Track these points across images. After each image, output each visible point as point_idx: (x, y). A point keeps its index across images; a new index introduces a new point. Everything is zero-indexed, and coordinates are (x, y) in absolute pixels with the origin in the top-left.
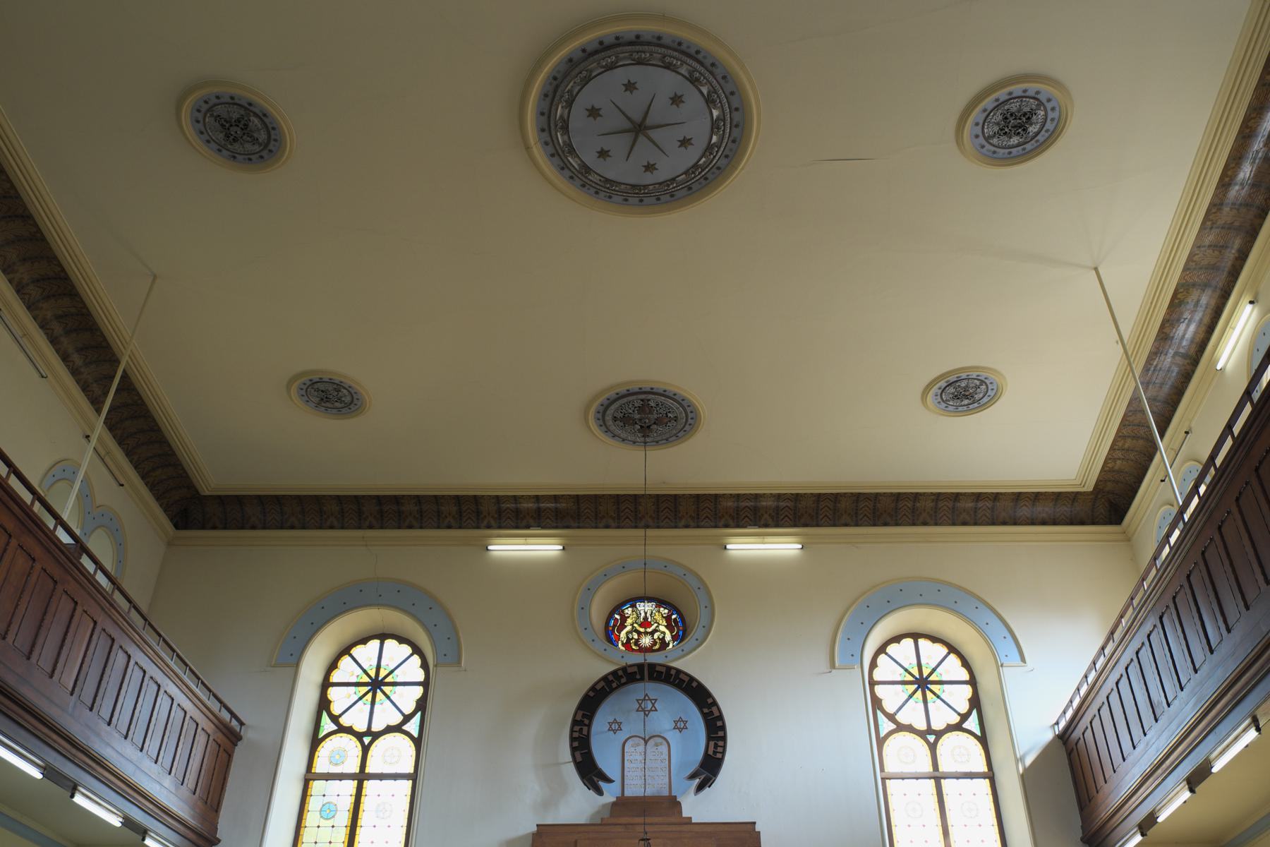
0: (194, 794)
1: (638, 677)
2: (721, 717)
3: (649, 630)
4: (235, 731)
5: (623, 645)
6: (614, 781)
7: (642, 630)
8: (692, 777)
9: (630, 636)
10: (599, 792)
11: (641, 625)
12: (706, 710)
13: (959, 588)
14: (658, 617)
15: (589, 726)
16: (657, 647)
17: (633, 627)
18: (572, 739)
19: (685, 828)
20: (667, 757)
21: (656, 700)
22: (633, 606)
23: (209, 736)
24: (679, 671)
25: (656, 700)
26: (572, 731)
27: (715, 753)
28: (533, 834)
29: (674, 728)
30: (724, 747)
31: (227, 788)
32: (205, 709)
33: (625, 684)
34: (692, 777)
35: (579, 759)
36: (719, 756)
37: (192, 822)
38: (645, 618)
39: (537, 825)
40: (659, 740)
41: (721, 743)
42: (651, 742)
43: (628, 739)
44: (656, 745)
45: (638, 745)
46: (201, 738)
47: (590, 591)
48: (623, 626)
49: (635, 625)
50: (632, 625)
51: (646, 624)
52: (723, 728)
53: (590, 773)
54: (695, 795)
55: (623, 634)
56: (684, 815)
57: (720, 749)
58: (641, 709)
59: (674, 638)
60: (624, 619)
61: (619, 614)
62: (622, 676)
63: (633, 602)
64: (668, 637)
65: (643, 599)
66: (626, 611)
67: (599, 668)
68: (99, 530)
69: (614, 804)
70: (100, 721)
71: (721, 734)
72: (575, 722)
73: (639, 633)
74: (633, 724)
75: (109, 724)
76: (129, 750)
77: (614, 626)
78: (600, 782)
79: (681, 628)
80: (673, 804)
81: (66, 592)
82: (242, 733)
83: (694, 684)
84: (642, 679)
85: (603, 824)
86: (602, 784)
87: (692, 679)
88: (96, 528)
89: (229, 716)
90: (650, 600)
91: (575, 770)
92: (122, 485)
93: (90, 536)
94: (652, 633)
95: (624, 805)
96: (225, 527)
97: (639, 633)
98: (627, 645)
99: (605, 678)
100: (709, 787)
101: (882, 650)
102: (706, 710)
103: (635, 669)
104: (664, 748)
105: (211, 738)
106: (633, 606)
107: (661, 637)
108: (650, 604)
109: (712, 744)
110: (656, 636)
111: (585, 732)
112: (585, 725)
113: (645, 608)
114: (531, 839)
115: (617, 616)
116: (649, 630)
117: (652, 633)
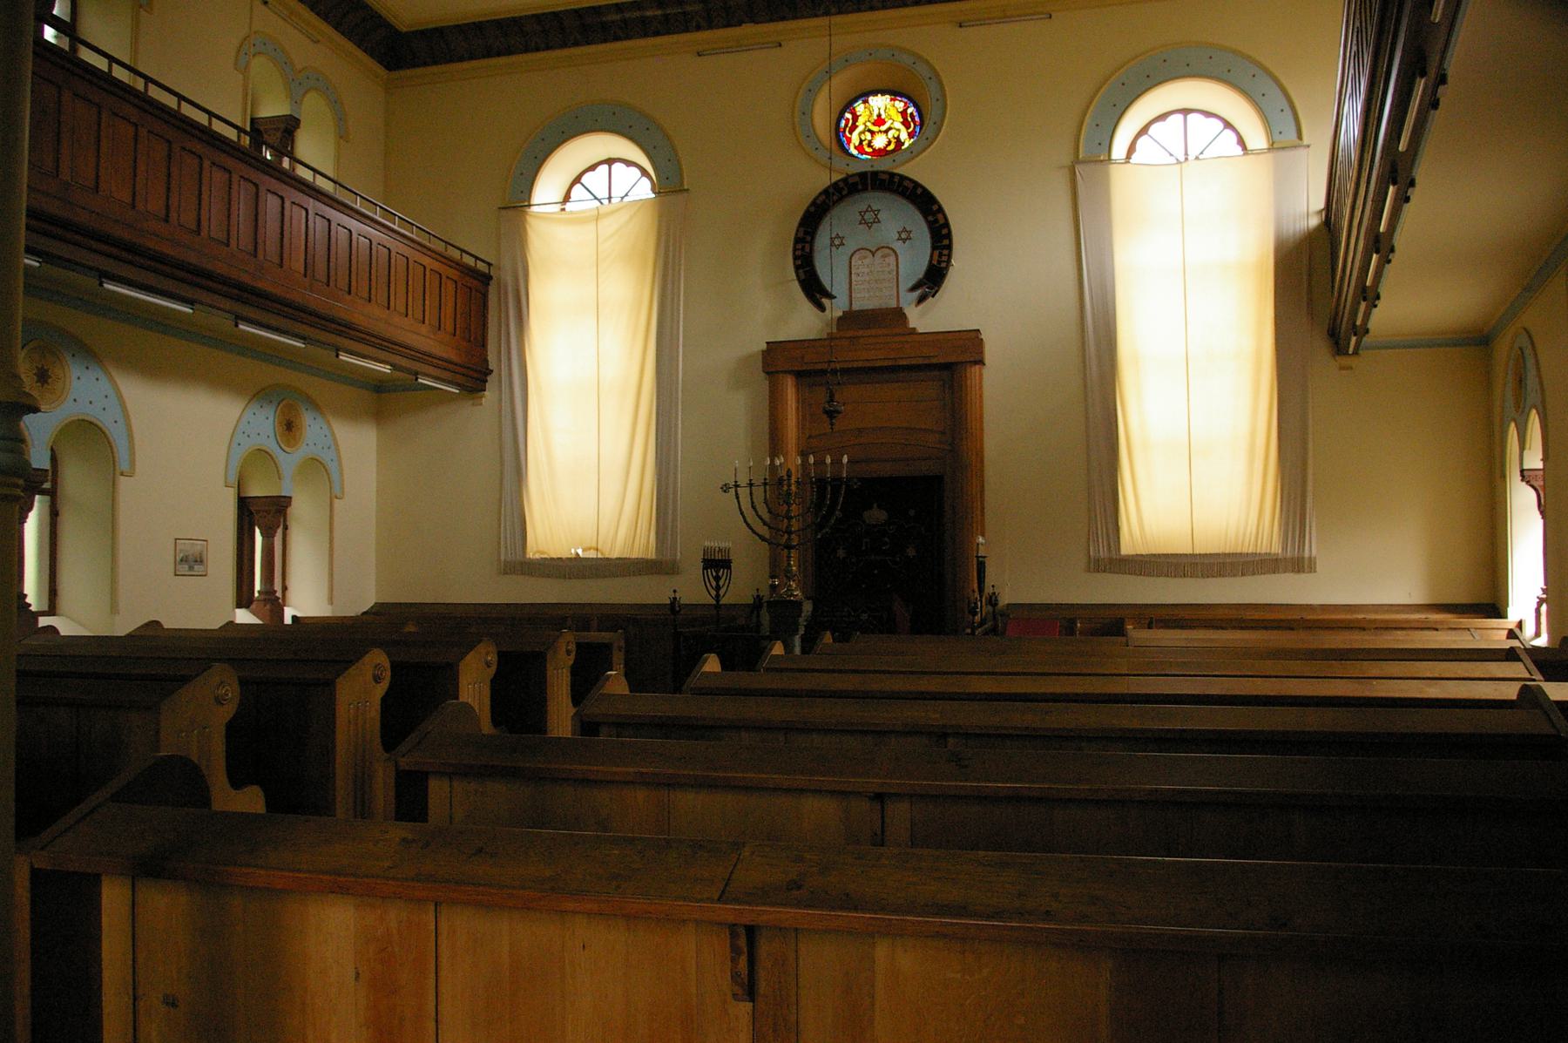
0: (455, 335)
1: (860, 187)
2: (947, 225)
3: (883, 128)
4: (485, 273)
5: (856, 148)
6: (836, 297)
7: (875, 129)
8: (913, 289)
9: (863, 138)
10: (822, 308)
11: (874, 124)
12: (930, 218)
13: (1235, 52)
14: (893, 113)
15: (812, 243)
16: (892, 147)
17: (866, 126)
18: (795, 258)
19: (908, 338)
20: (895, 268)
21: (879, 211)
22: (865, 102)
23: (456, 282)
24: (903, 178)
25: (879, 211)
26: (795, 250)
27: (939, 262)
28: (763, 351)
29: (898, 239)
30: (950, 256)
31: (489, 325)
32: (443, 260)
33: (847, 195)
34: (913, 289)
35: (803, 277)
36: (943, 265)
37: (454, 357)
38: (879, 116)
39: (768, 343)
40: (887, 251)
41: (945, 252)
42: (879, 253)
43: (855, 252)
44: (884, 256)
45: (865, 258)
46: (451, 287)
47: (812, 93)
48: (854, 127)
49: (868, 124)
50: (864, 124)
51: (880, 121)
52: (949, 236)
53: (814, 290)
54: (916, 306)
55: (855, 134)
56: (911, 326)
57: (944, 258)
58: (863, 222)
59: (911, 135)
60: (855, 118)
61: (851, 113)
62: (843, 188)
63: (864, 96)
64: (904, 136)
65: (875, 93)
66: (857, 109)
67: (823, 180)
68: (308, 96)
69: (840, 319)
70: (340, 293)
71: (946, 242)
72: (797, 240)
73: (873, 133)
74: (857, 237)
75: (349, 293)
76: (376, 311)
77: (846, 125)
78: (823, 300)
79: (922, 121)
80: (898, 315)
81: (269, 190)
82: (492, 274)
83: (919, 191)
84: (865, 189)
85: (831, 337)
86: (825, 301)
87: (917, 185)
88: (306, 92)
89: (473, 260)
90: (883, 93)
91: (800, 290)
92: (318, 41)
93: (301, 104)
94: (886, 132)
95: (851, 319)
96: (435, 62)
97: (873, 133)
98: (860, 148)
99: (826, 192)
100: (933, 296)
101: (1144, 131)
102: (930, 218)
103: (857, 179)
104: (892, 259)
105: (459, 285)
106: (865, 102)
107: (896, 136)
108: (884, 98)
109: (937, 252)
110: (891, 134)
111: (807, 250)
112: (807, 242)
113: (879, 103)
114: (760, 357)
115: (848, 116)
116: (883, 128)
117: (886, 132)
